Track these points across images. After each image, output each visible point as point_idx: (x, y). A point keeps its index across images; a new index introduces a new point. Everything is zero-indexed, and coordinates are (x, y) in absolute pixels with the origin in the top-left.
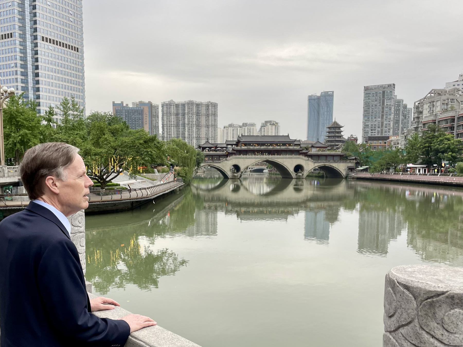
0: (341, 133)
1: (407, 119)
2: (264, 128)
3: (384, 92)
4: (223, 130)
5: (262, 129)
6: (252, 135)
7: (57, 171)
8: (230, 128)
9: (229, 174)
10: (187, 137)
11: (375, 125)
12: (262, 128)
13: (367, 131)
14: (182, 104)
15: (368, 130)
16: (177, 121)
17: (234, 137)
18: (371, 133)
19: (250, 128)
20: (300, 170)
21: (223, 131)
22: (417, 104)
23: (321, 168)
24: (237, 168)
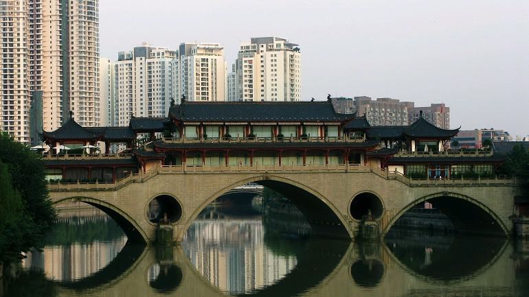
4: (117, 66)
7: (226, 217)
8: (138, 59)
9: (145, 227)
21: (117, 70)
23: (443, 203)
24: (167, 207)
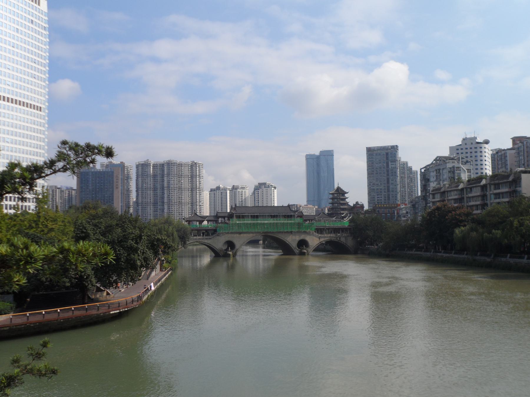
0: (346, 200)
1: (413, 183)
2: (258, 192)
3: (387, 154)
5: (256, 193)
6: (244, 206)
8: (217, 191)
10: (167, 203)
11: (381, 189)
12: (256, 191)
13: (373, 196)
14: (161, 164)
15: (373, 195)
16: (155, 209)
17: (223, 208)
18: (377, 198)
19: (241, 191)
20: (304, 246)
22: (423, 171)
